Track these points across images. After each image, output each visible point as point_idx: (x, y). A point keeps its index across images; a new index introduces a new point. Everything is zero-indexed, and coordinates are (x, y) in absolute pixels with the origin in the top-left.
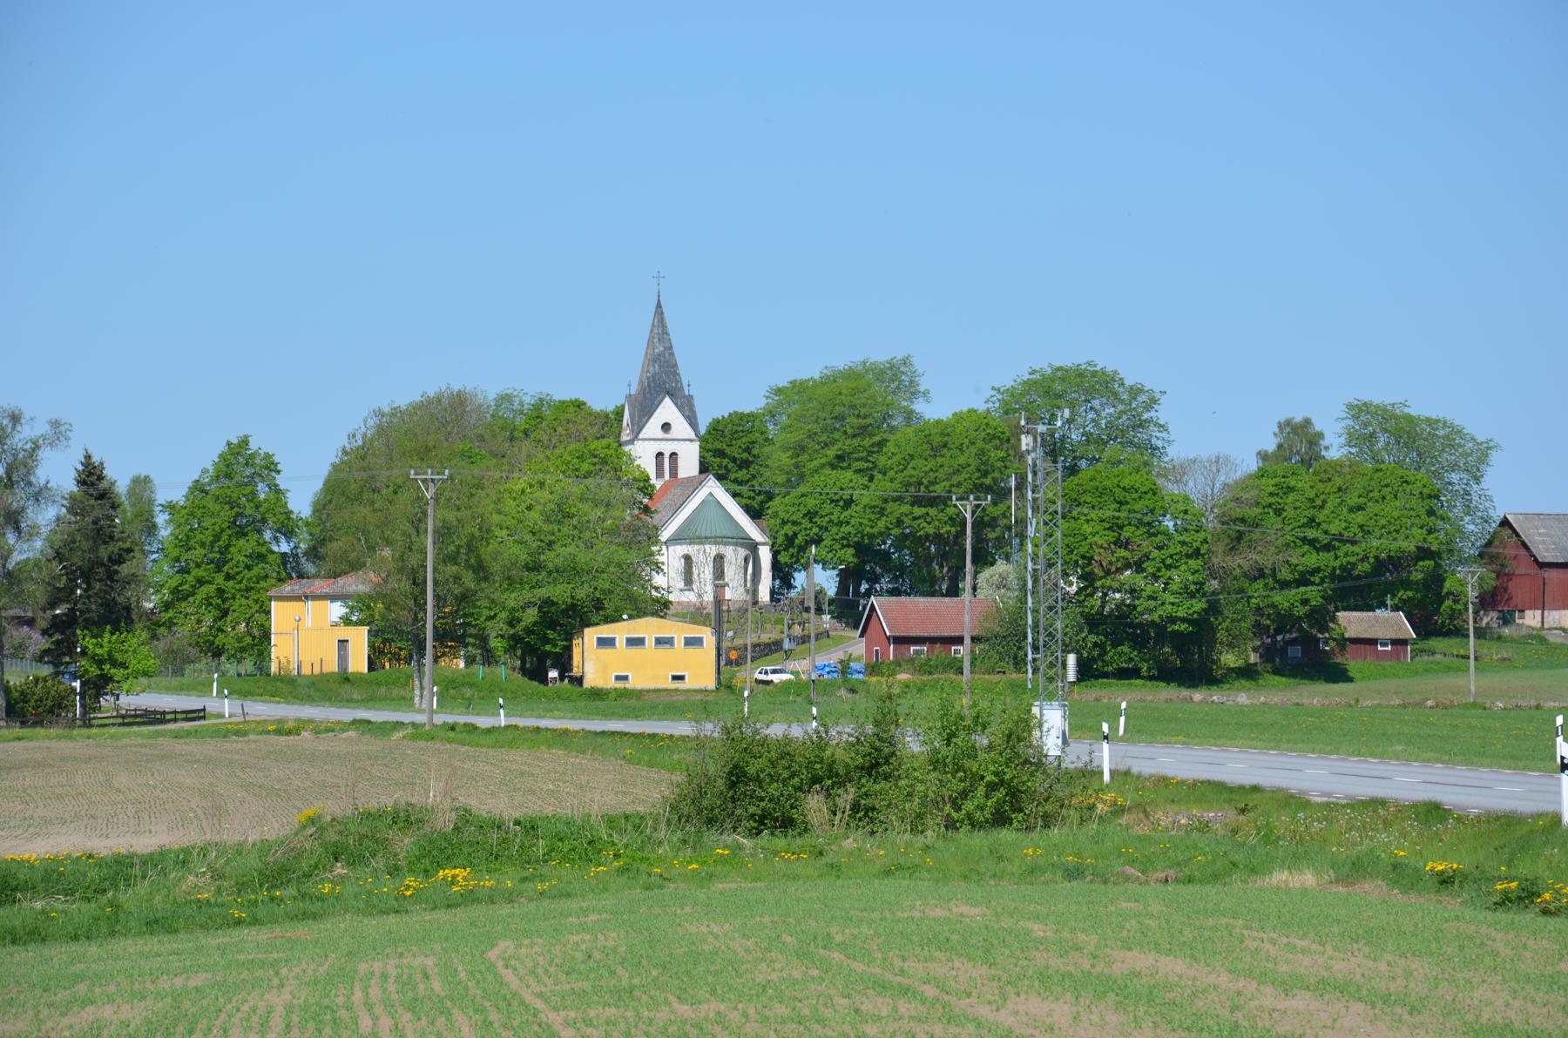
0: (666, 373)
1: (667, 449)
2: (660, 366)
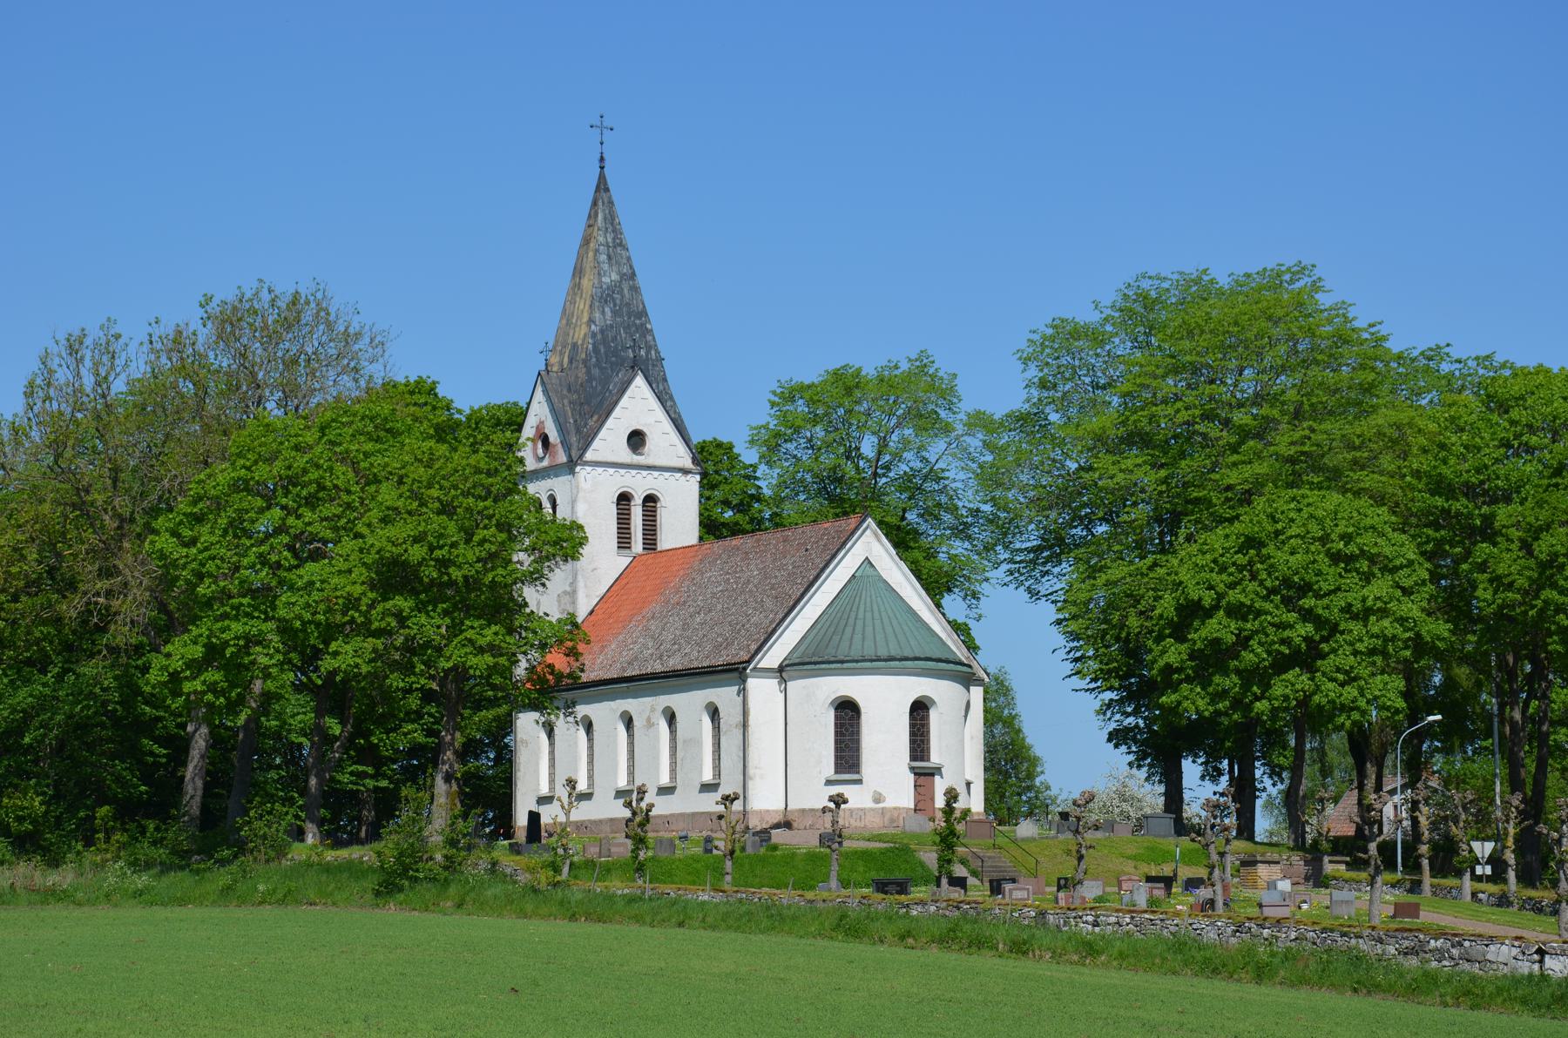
0: (628, 327)
1: (640, 485)
2: (615, 313)
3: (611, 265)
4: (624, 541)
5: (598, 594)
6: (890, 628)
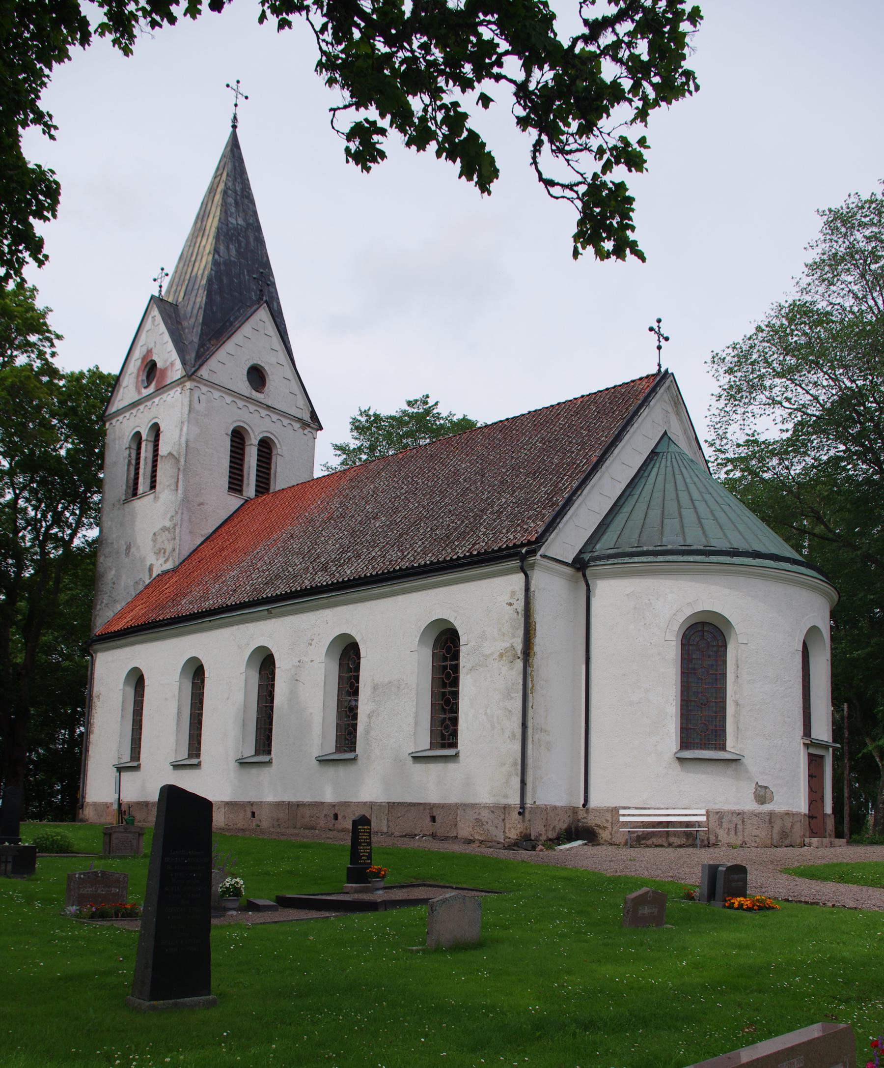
3: (237, 210)
4: (236, 484)
5: (203, 532)
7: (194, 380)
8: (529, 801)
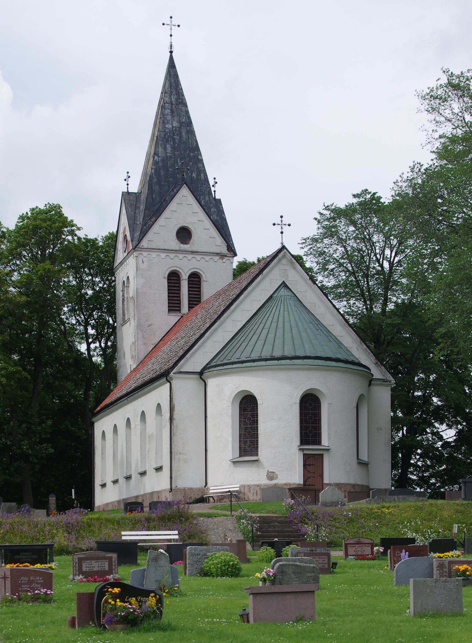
2: (174, 148)
5: (153, 342)
6: (290, 335)
7: (137, 251)
8: (174, 486)
